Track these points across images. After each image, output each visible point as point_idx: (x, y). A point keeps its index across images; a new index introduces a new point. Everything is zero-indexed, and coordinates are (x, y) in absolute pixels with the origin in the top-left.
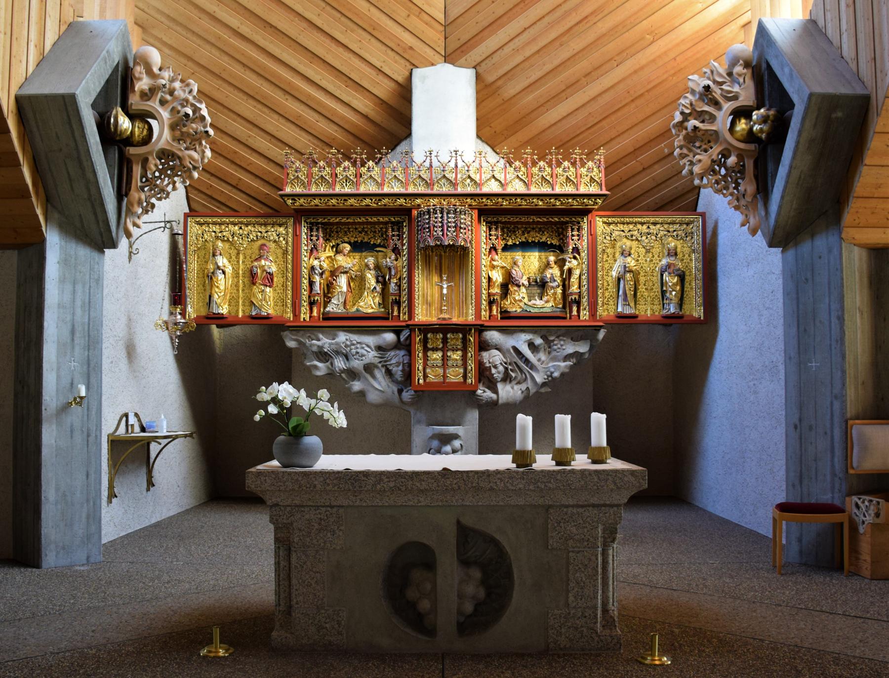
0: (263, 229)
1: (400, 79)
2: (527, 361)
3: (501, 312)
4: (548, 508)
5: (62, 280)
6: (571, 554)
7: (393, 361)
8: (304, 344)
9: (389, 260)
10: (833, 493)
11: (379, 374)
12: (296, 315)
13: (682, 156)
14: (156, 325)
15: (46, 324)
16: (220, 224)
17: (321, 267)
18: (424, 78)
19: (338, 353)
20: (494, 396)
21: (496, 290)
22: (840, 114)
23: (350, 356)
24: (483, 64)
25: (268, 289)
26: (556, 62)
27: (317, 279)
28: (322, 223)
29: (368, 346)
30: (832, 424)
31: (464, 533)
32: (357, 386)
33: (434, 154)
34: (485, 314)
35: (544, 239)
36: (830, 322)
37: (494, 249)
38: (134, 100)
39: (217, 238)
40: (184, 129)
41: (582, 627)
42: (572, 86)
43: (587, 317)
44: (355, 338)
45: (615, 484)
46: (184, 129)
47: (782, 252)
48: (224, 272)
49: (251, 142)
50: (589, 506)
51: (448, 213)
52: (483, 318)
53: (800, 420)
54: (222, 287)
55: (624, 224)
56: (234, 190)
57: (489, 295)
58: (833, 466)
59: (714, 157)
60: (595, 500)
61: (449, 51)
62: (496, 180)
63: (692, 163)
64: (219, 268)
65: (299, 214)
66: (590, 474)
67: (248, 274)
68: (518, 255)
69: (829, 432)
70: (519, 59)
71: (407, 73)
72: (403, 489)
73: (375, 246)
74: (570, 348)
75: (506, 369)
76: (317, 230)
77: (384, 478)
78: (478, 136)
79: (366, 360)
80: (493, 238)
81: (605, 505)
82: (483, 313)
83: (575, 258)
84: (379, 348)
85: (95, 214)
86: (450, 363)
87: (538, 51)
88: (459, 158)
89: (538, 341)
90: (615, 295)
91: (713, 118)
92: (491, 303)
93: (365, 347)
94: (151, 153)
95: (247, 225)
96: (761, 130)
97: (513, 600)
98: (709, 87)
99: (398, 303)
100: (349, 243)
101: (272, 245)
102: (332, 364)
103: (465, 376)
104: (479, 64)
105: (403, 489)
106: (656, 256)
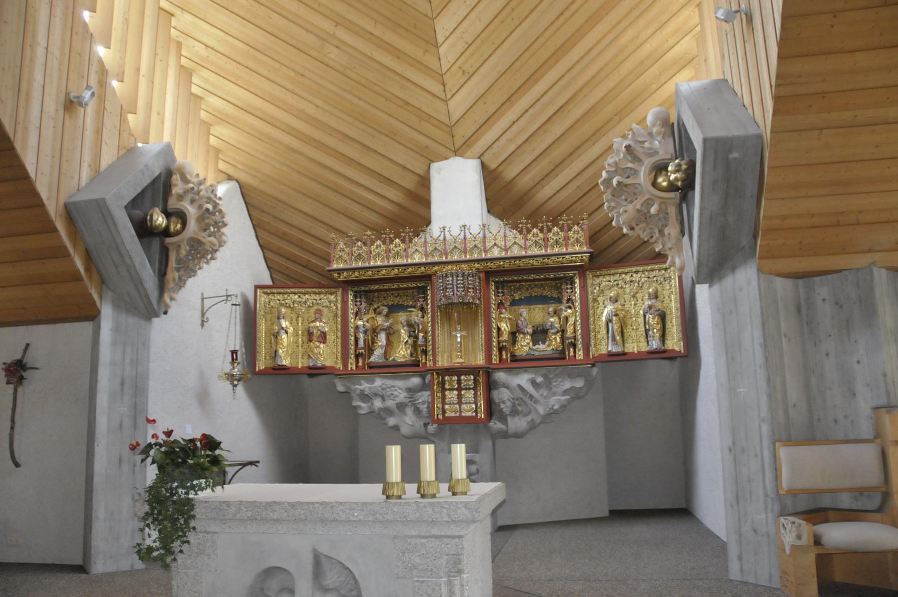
0: (317, 297)
1: (421, 172)
2: (531, 397)
5: (114, 343)
7: (420, 401)
8: (349, 388)
9: (416, 316)
11: (409, 411)
12: (345, 365)
13: (611, 209)
14: (219, 376)
15: (99, 378)
16: (283, 294)
18: (439, 171)
19: (376, 395)
21: (505, 337)
23: (386, 398)
25: (322, 346)
26: (544, 146)
27: (361, 336)
28: (364, 291)
29: (400, 389)
31: (318, 560)
32: (392, 421)
33: (447, 229)
34: (495, 359)
36: (754, 350)
38: (172, 203)
39: (282, 305)
42: (559, 166)
43: (582, 357)
44: (389, 382)
45: (449, 516)
48: (287, 332)
49: (313, 232)
50: (431, 537)
52: (494, 362)
54: (285, 344)
57: (499, 342)
59: (638, 207)
61: (457, 145)
62: (498, 247)
63: (619, 215)
64: (282, 328)
65: (348, 284)
67: (306, 334)
68: (524, 310)
70: (513, 147)
71: (426, 168)
72: (259, 518)
73: (408, 307)
75: (514, 404)
77: (243, 507)
78: (489, 212)
79: (398, 400)
81: (447, 537)
82: (494, 357)
83: (570, 308)
84: (409, 390)
85: (138, 290)
87: (527, 140)
89: (539, 379)
90: (605, 337)
92: (500, 350)
93: (398, 388)
94: (182, 241)
95: (305, 294)
98: (629, 146)
99: (425, 352)
100: (387, 306)
102: (372, 404)
103: (476, 411)
104: (482, 155)
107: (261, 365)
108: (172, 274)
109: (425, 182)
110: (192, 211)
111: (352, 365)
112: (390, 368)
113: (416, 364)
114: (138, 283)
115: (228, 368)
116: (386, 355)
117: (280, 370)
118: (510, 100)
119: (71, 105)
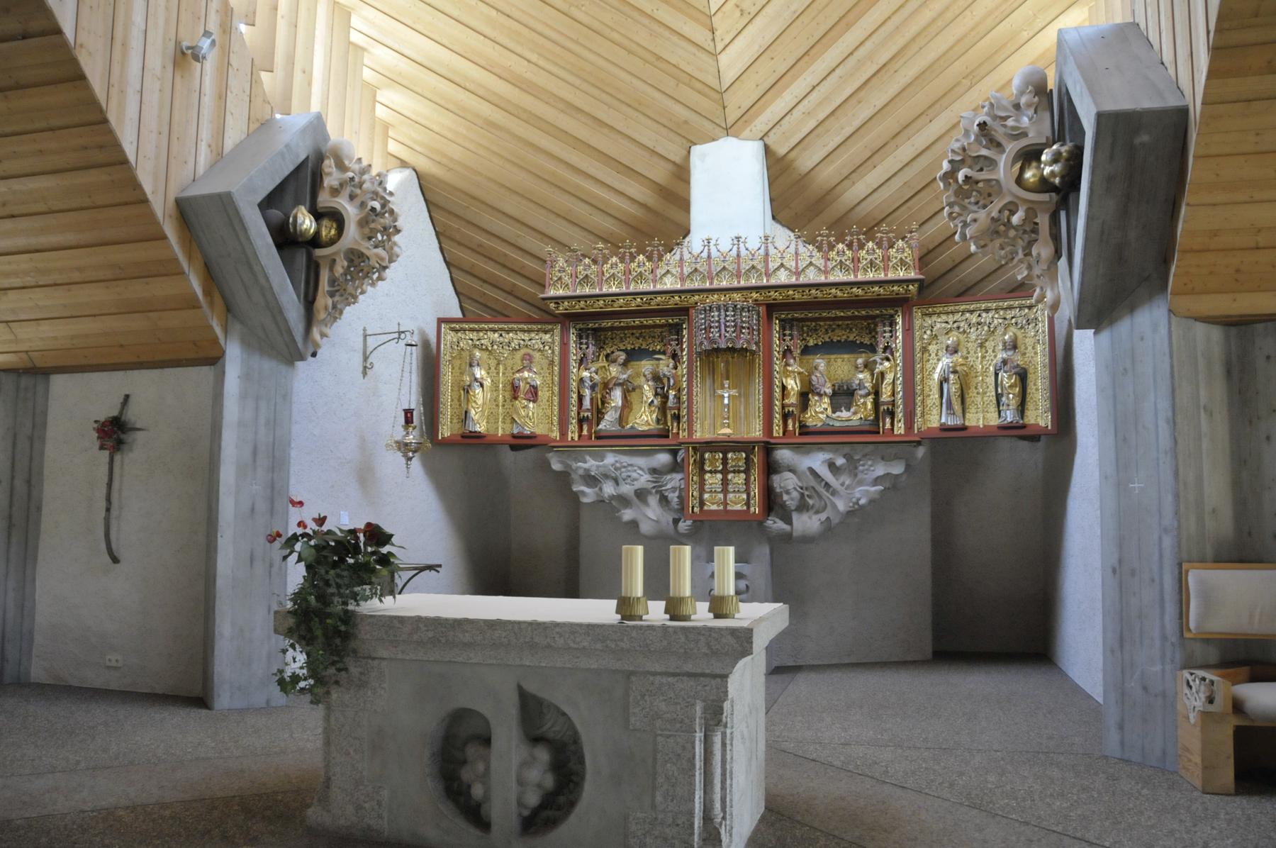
0: (526, 337)
1: (677, 159)
3: (801, 427)
4: (629, 674)
5: (243, 396)
6: (659, 738)
7: (669, 486)
9: (665, 366)
10: (1163, 664)
11: (653, 500)
12: (563, 433)
14: (387, 445)
15: (224, 444)
17: (591, 379)
19: (606, 476)
20: (787, 527)
22: (1145, 138)
23: (620, 481)
24: (771, 134)
25: (531, 405)
26: (857, 123)
27: (587, 392)
28: (593, 329)
29: (641, 469)
30: (1161, 568)
32: (627, 515)
33: (713, 242)
34: (777, 430)
35: (851, 338)
37: (787, 353)
38: (324, 200)
39: (475, 346)
40: (372, 225)
41: (673, 838)
42: (879, 151)
43: (902, 431)
44: (626, 460)
45: (709, 647)
46: (372, 225)
47: (1095, 333)
48: (482, 385)
50: (684, 675)
51: (727, 310)
52: (775, 434)
53: (1120, 561)
54: (480, 402)
55: (947, 313)
56: (511, 297)
57: (783, 407)
58: (1163, 627)
59: (995, 214)
60: (689, 667)
61: (730, 121)
62: (787, 269)
64: (476, 380)
66: (675, 632)
67: (509, 388)
68: (820, 362)
69: (1157, 578)
71: (685, 152)
72: (443, 640)
73: (655, 352)
74: (880, 470)
75: (802, 495)
76: (587, 338)
78: (774, 218)
79: (638, 485)
80: (788, 338)
81: (703, 675)
83: (888, 359)
84: (654, 471)
85: (277, 323)
86: (730, 488)
87: (833, 113)
88: (741, 245)
89: (840, 461)
90: (938, 403)
91: (992, 163)
92: (785, 417)
93: (637, 470)
95: (508, 332)
96: (1052, 172)
97: (585, 795)
99: (677, 418)
101: (537, 355)
102: (601, 489)
103: (748, 504)
104: (766, 134)
105: (443, 640)
106: (990, 351)
107: (445, 431)
108: (323, 301)
109: (682, 173)
110: (351, 212)
111: (573, 434)
112: (629, 440)
113: (664, 434)
114: (276, 311)
115: (399, 433)
116: (621, 420)
117: (477, 436)
118: (808, 55)
119: (184, 57)
